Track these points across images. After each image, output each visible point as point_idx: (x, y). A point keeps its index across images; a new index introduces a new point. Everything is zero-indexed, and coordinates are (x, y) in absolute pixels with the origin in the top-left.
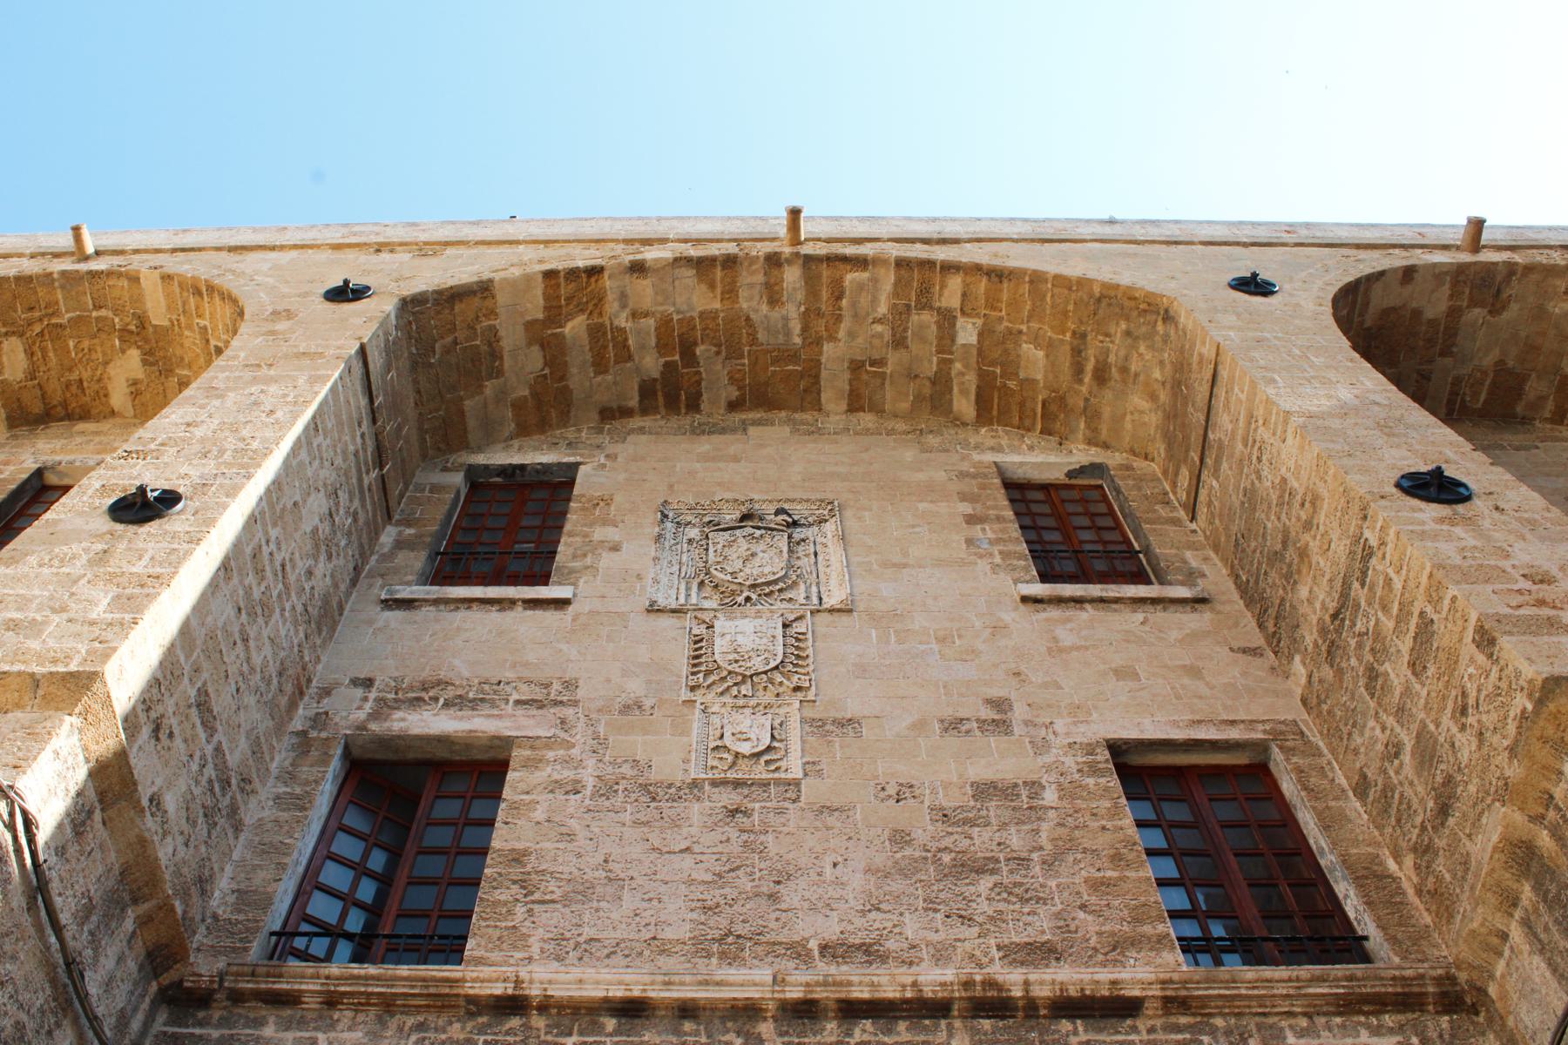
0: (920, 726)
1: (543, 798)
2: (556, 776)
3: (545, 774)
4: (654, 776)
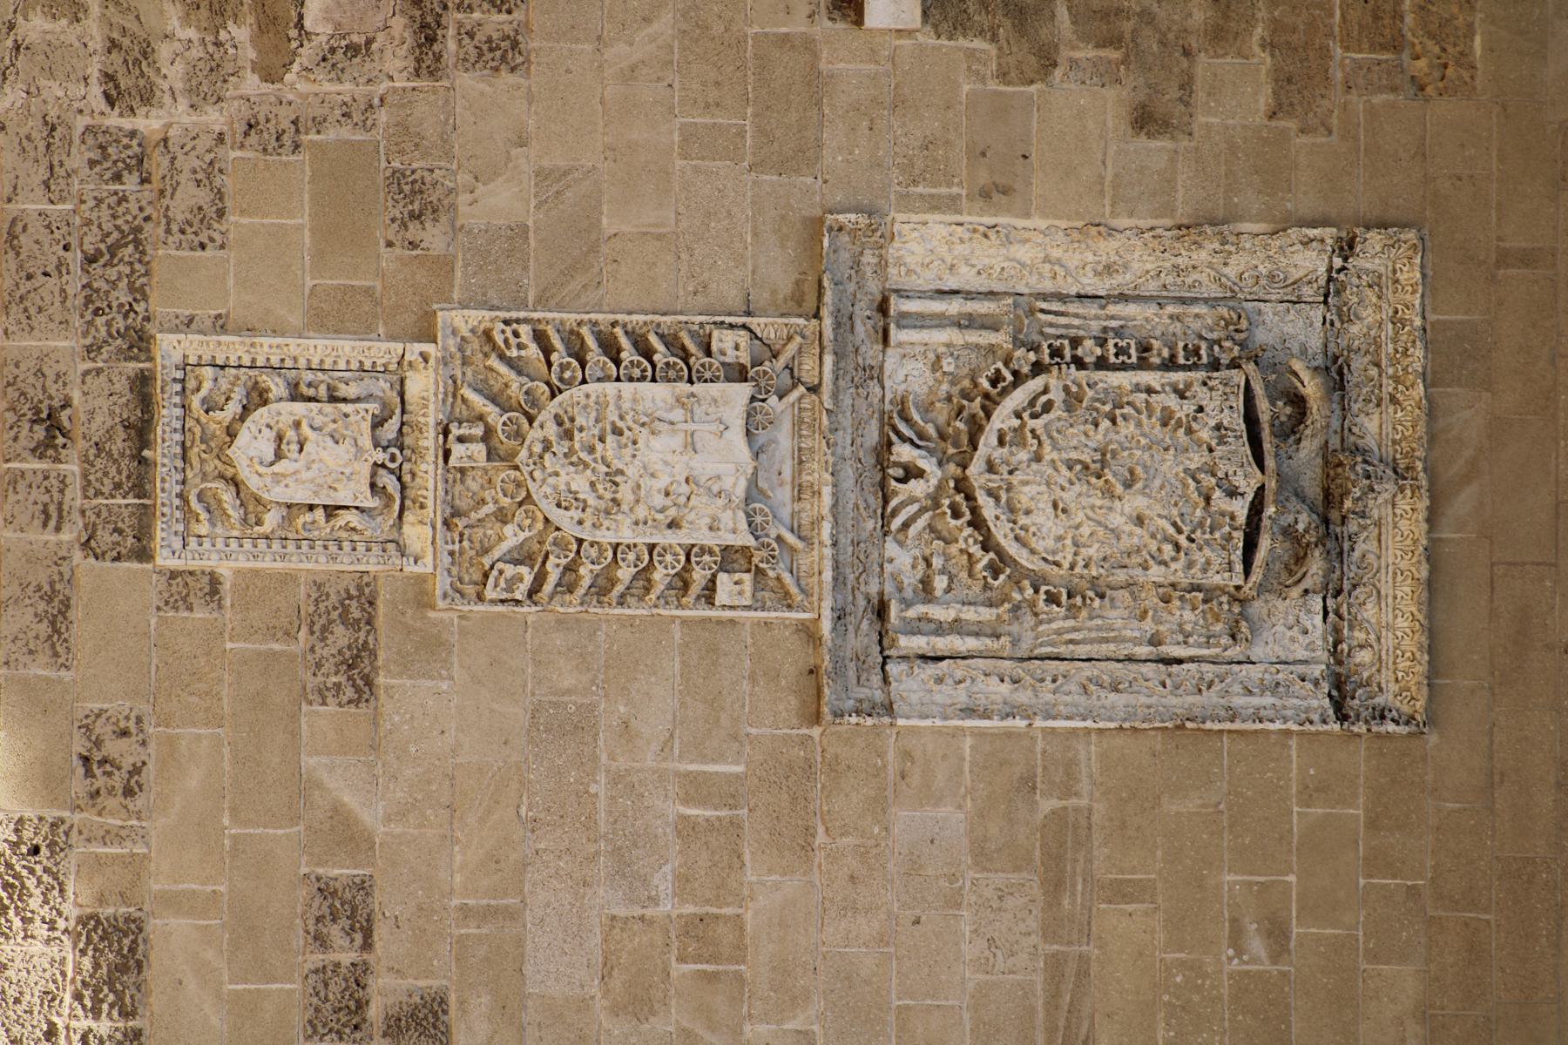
0: (345, 834)
1: (94, 30)
2: (164, 51)
3: (174, 23)
4: (165, 254)
